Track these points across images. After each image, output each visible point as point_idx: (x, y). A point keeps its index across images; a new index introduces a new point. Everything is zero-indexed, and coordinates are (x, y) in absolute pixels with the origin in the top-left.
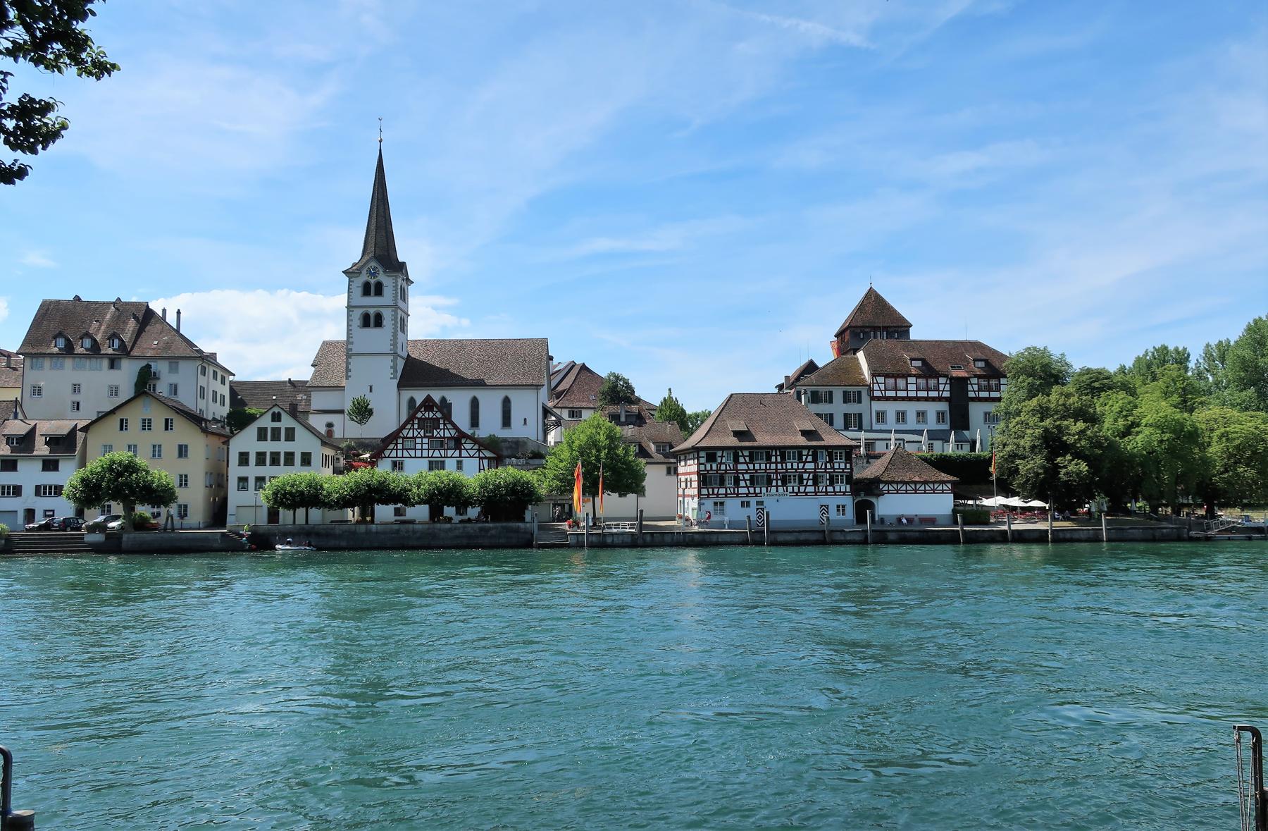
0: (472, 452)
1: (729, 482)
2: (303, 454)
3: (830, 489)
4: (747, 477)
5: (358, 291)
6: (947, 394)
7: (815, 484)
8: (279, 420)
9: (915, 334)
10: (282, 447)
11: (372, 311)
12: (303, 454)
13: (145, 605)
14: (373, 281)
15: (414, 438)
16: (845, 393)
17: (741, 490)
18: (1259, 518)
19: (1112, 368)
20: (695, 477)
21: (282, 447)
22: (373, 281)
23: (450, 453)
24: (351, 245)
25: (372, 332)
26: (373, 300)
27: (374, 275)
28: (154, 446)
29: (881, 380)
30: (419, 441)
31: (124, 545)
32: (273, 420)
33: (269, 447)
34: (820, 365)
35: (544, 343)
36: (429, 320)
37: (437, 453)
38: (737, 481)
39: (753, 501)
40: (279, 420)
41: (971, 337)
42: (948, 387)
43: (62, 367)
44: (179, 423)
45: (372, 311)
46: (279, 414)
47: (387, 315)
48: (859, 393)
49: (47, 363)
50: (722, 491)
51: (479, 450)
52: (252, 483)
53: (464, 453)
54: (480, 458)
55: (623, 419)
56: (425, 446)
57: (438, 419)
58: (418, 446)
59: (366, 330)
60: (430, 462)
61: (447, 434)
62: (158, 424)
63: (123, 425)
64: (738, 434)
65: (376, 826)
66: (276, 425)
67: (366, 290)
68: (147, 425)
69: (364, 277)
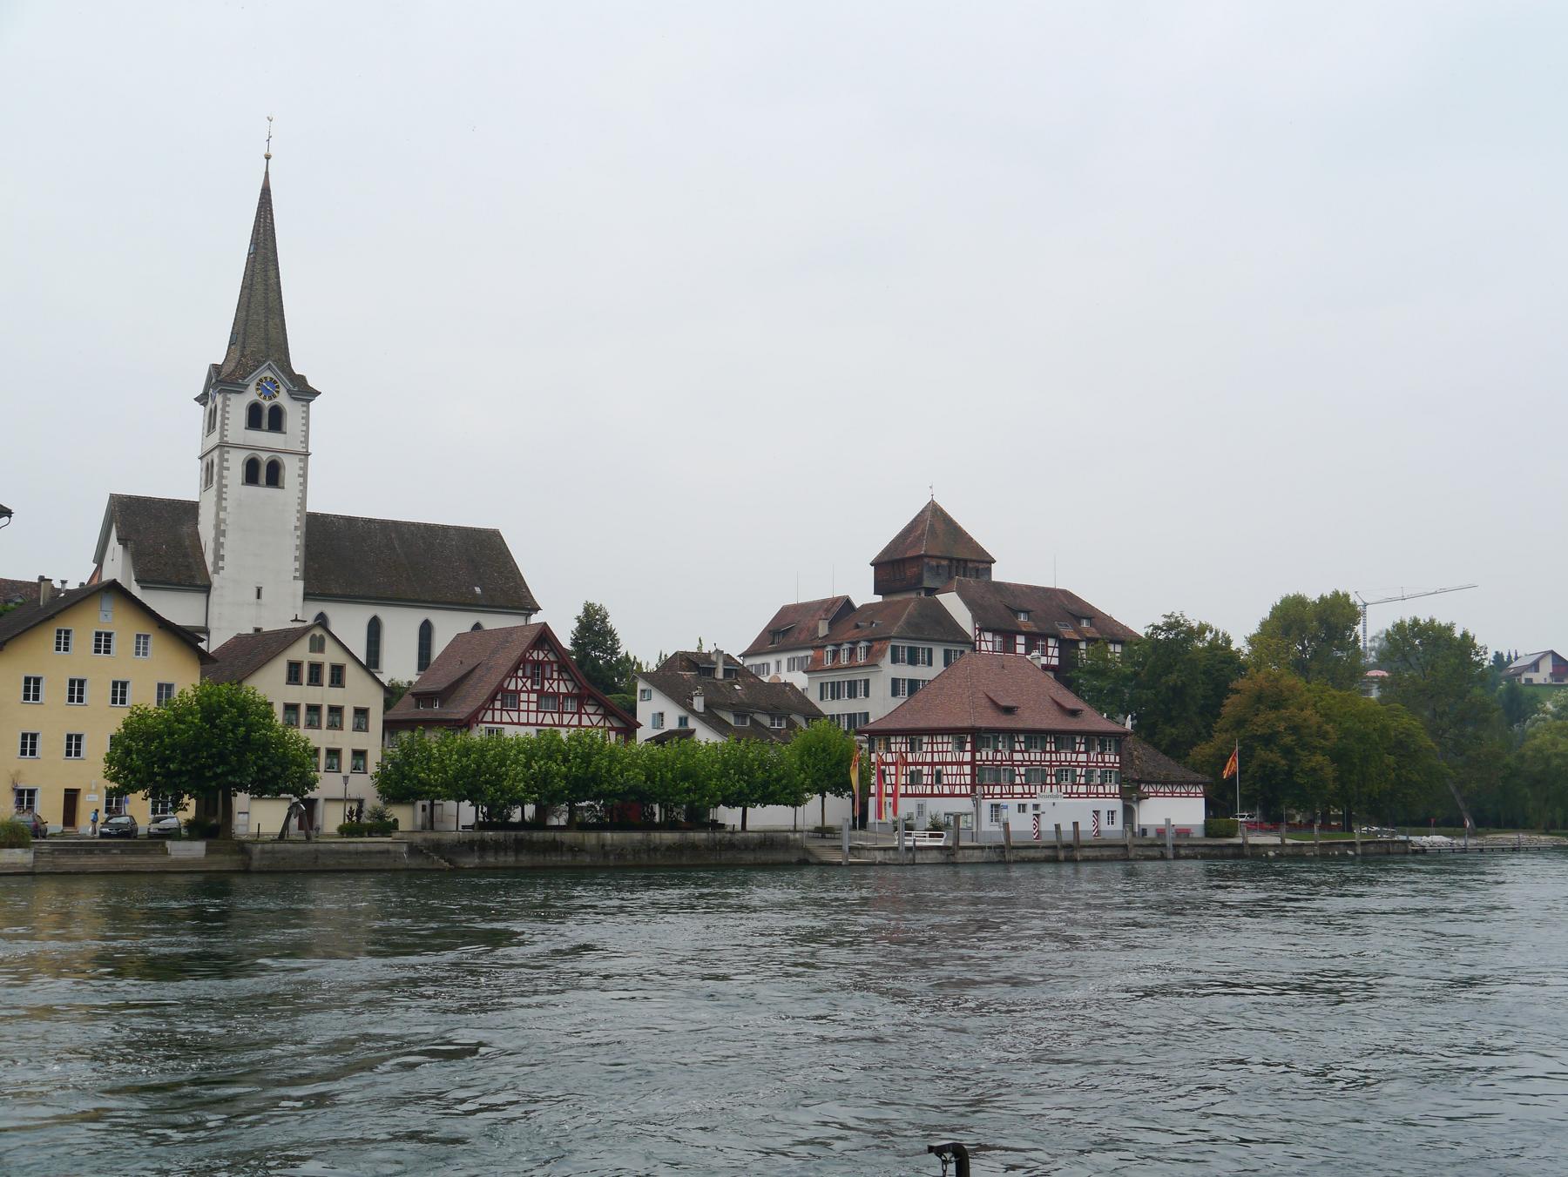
0: (595, 719)
1: (1004, 777)
3: (1101, 789)
4: (1022, 770)
6: (1055, 662)
9: (999, 574)
10: (325, 695)
11: (265, 457)
14: (267, 404)
15: (518, 692)
17: (1018, 789)
21: (325, 695)
22: (267, 404)
23: (566, 718)
25: (262, 492)
26: (264, 438)
29: (989, 636)
30: (524, 696)
31: (255, 864)
32: (312, 650)
33: (304, 694)
34: (857, 605)
35: (112, 497)
38: (1013, 774)
39: (1030, 802)
41: (1060, 586)
42: (1056, 653)
44: (158, 645)
45: (265, 457)
46: (322, 638)
47: (290, 467)
50: (997, 789)
52: (347, 760)
56: (533, 707)
57: (550, 663)
58: (523, 706)
59: (252, 489)
61: (563, 690)
66: (317, 657)
68: (103, 642)
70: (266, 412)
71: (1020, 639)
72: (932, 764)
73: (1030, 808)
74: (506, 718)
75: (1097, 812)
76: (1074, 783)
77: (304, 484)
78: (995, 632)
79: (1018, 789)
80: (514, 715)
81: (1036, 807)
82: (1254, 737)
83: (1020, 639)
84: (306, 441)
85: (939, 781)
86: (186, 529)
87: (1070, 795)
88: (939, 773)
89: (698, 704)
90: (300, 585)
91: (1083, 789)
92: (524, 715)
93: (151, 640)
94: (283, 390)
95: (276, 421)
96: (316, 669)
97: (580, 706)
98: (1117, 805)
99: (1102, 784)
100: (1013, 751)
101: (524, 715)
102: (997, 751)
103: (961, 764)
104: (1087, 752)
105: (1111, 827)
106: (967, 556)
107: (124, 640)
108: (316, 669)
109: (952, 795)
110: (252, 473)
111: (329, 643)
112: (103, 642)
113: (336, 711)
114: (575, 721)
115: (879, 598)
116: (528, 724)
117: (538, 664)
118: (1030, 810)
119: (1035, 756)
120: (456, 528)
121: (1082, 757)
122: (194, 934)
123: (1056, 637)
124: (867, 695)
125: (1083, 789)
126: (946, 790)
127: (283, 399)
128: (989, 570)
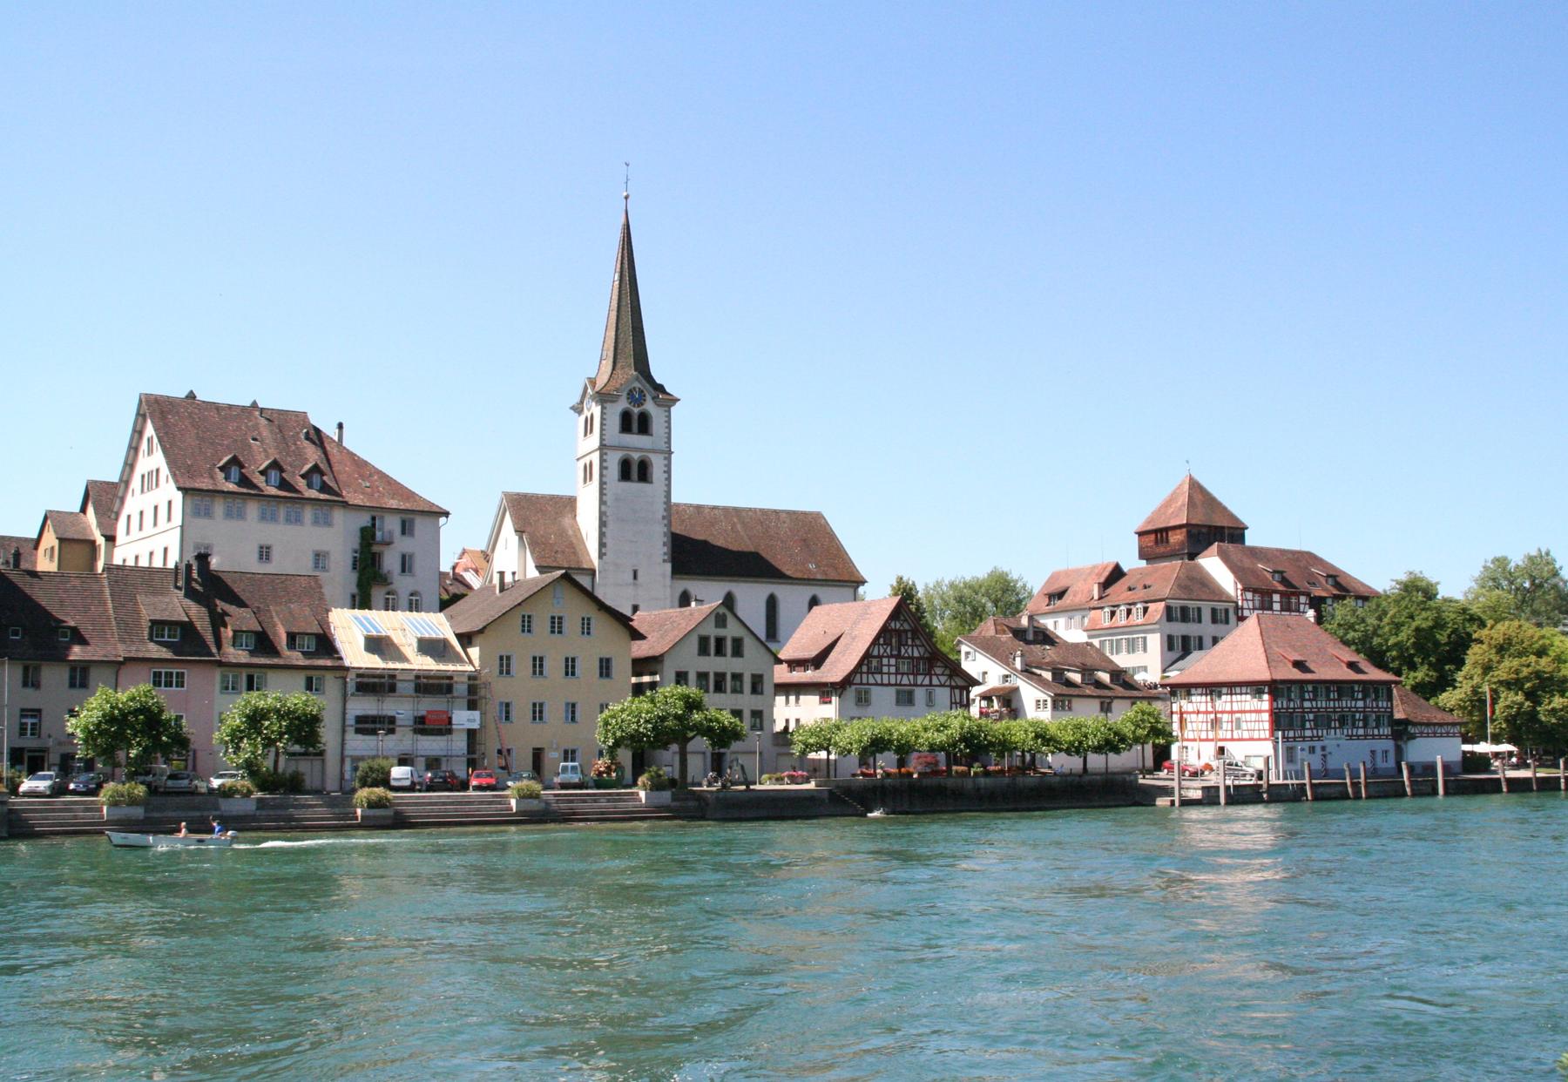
0: (943, 679)
1: (1297, 722)
2: (753, 676)
4: (1311, 716)
5: (615, 422)
7: (1365, 727)
8: (724, 626)
9: (1251, 539)
10: (728, 664)
11: (636, 456)
12: (753, 676)
13: (56, 973)
14: (636, 410)
16: (1214, 611)
17: (1308, 733)
18: (2, 927)
19: (1380, 590)
20: (1266, 716)
21: (728, 664)
22: (636, 410)
23: (920, 679)
24: (588, 354)
25: (634, 487)
27: (639, 401)
28: (501, 658)
30: (885, 661)
35: (506, 495)
36: (712, 471)
37: (905, 681)
38: (1303, 721)
39: (1318, 745)
40: (724, 626)
43: (241, 516)
44: (600, 623)
45: (636, 456)
47: (657, 463)
48: (1227, 611)
49: (219, 507)
51: (950, 677)
53: (935, 681)
54: (952, 688)
55: (1030, 637)
56: (893, 670)
57: (906, 631)
58: (885, 669)
60: (898, 692)
61: (916, 654)
62: (572, 625)
63: (527, 625)
64: (1299, 665)
65: (1499, 1078)
66: (721, 632)
67: (626, 423)
68: (557, 625)
69: (623, 404)
70: (635, 418)
71: (1276, 597)
72: (1232, 712)
73: (1318, 750)
74: (871, 681)
75: (1373, 752)
76: (1354, 726)
77: (669, 479)
78: (1255, 591)
79: (1308, 733)
80: (878, 677)
81: (1323, 748)
82: (1501, 682)
83: (1276, 597)
84: (669, 442)
85: (1238, 727)
86: (567, 521)
87: (1350, 737)
88: (1238, 720)
89: (1018, 664)
90: (668, 566)
91: (1361, 732)
92: (885, 677)
93: (593, 622)
94: (648, 398)
95: (644, 425)
96: (720, 642)
97: (931, 667)
98: (1389, 745)
99: (1377, 727)
100: (1303, 699)
101: (885, 677)
102: (1290, 700)
103: (1259, 712)
104: (1364, 699)
105: (1385, 765)
106: (1225, 524)
107: (572, 625)
108: (720, 642)
109: (1252, 739)
110: (626, 471)
111: (730, 619)
112: (557, 625)
113: (737, 677)
114: (927, 681)
115: (1143, 563)
116: (889, 685)
117: (898, 633)
118: (1318, 751)
119: (1322, 704)
120: (789, 513)
121: (1360, 704)
122: (616, 855)
123: (1308, 594)
124: (1145, 650)
125: (1361, 732)
126: (1246, 735)
127: (649, 406)
128: (1243, 536)
